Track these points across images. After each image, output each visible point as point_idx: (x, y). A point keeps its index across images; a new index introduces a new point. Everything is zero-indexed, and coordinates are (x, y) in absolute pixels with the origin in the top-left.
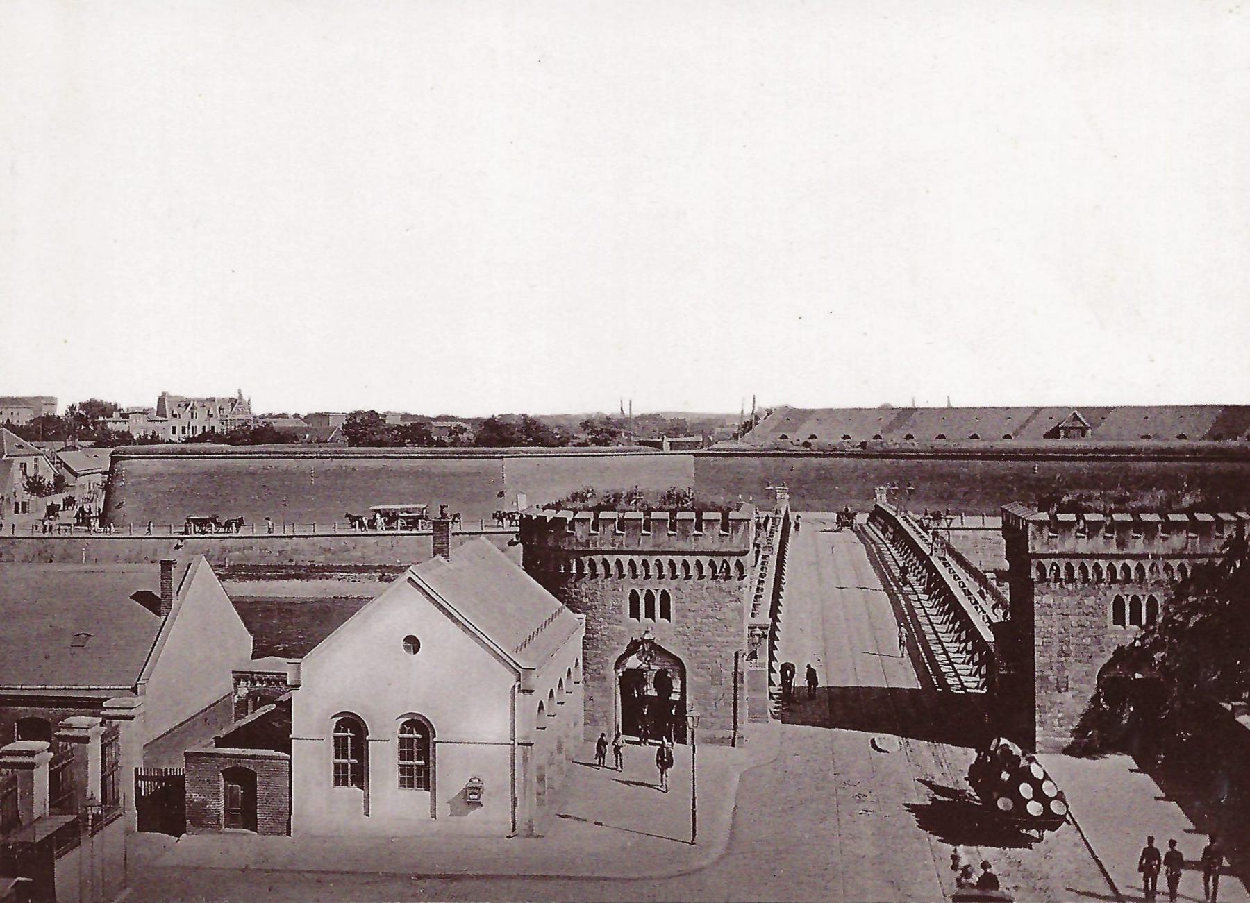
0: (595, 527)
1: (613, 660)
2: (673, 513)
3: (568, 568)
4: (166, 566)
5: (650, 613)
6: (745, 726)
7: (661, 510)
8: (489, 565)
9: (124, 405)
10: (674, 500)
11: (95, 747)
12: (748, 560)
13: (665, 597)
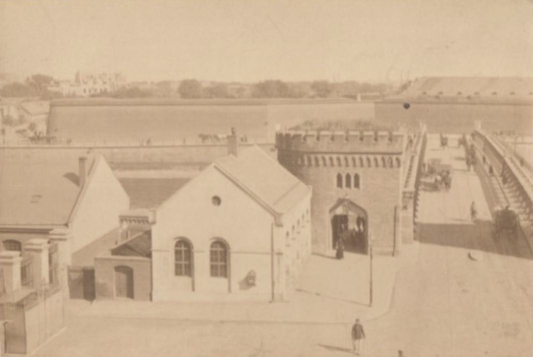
0: (318, 138)
1: (328, 208)
2: (362, 132)
3: (303, 161)
4: (82, 160)
5: (348, 185)
6: (400, 246)
7: (355, 130)
8: (260, 164)
9: (56, 77)
10: (362, 125)
11: (44, 257)
12: (402, 158)
13: (357, 177)
